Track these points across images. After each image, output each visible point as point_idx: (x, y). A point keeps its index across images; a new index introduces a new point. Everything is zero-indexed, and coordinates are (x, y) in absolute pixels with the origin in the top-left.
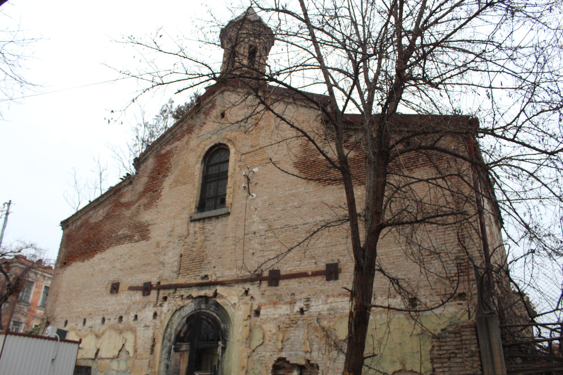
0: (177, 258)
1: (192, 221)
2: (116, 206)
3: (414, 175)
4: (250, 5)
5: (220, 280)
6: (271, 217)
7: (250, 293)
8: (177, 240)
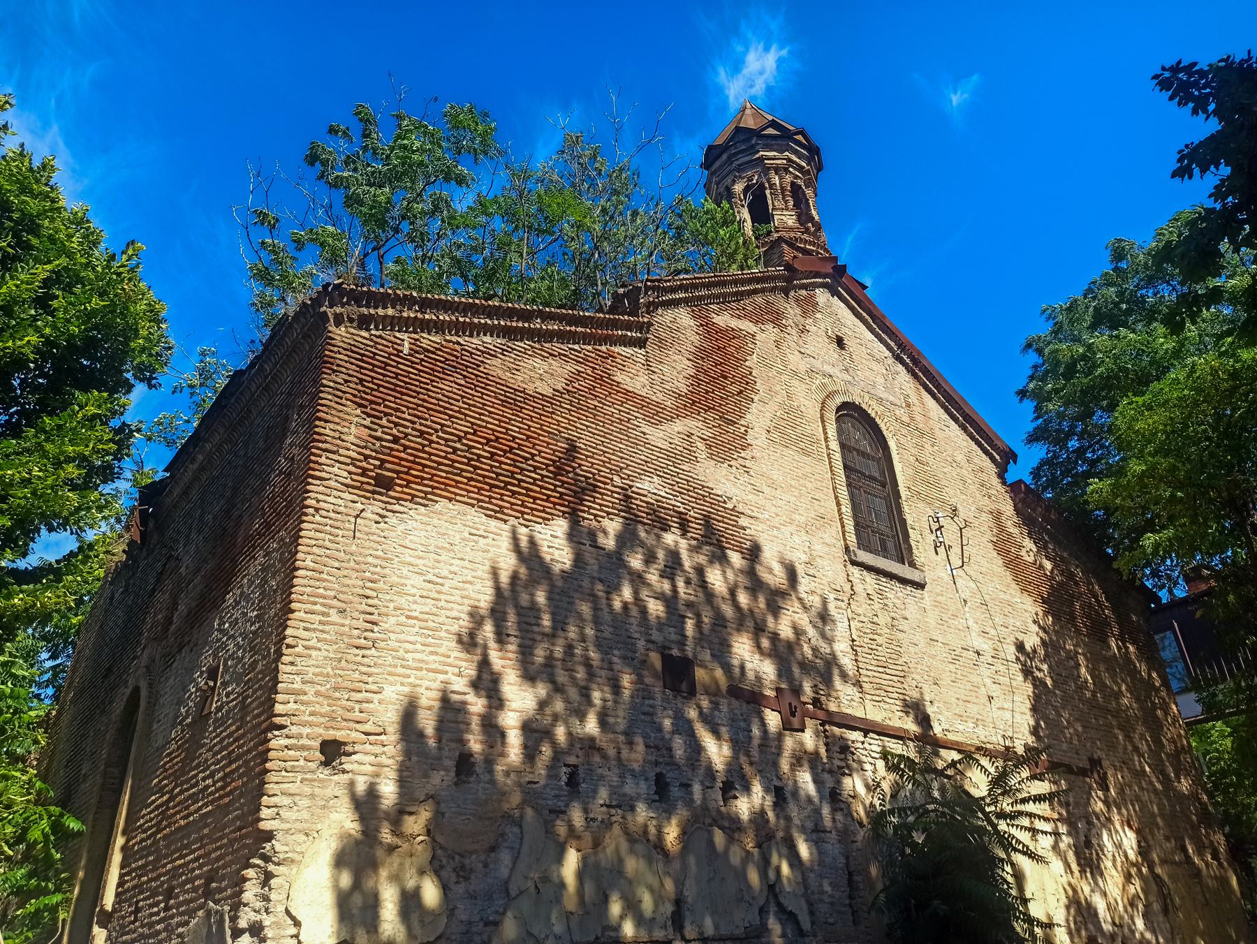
5: (951, 737)
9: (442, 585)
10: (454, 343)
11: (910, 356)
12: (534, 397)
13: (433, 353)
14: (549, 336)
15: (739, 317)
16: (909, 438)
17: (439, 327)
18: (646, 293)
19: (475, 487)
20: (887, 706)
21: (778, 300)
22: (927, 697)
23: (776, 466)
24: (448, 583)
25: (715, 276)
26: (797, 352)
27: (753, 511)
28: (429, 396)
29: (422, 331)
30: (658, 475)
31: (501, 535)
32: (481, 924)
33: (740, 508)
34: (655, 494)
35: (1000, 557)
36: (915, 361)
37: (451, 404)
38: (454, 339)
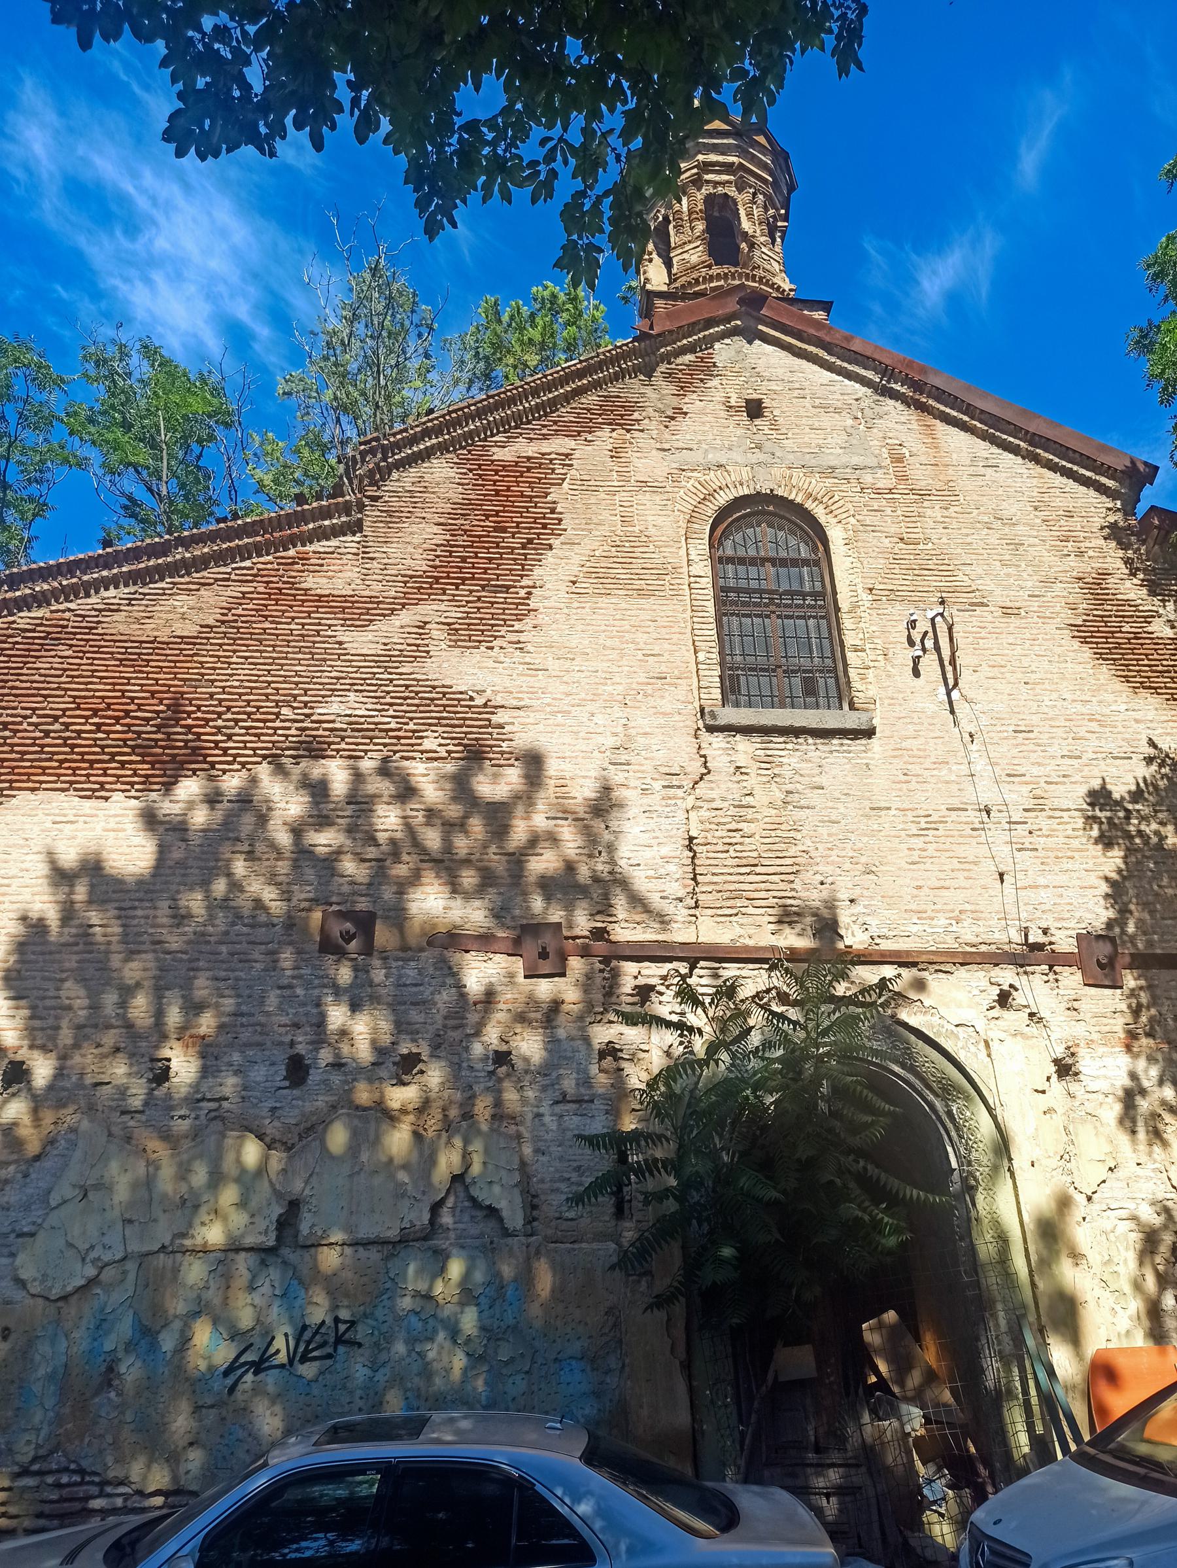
0: (675, 848)
1: (711, 729)
2: (275, 595)
3: (317, 1364)
4: (1109, 1230)
5: (886, 945)
6: (1036, 771)
7: (1019, 998)
8: (657, 785)
9: (8, 886)
10: (63, 611)
11: (907, 381)
12: (168, 643)
13: (34, 631)
14: (202, 563)
15: (545, 437)
16: (888, 511)
17: (41, 600)
18: (363, 461)
19: (69, 768)
20: (750, 920)
21: (633, 387)
22: (843, 895)
23: (580, 627)
24: (15, 883)
25: (489, 397)
26: (654, 452)
27: (521, 699)
28: (22, 681)
29: (20, 610)
30: (356, 691)
31: (96, 816)
32: (13, 1236)
33: (498, 700)
34: (350, 716)
35: (1086, 647)
36: (918, 386)
37: (49, 683)
38: (61, 607)
